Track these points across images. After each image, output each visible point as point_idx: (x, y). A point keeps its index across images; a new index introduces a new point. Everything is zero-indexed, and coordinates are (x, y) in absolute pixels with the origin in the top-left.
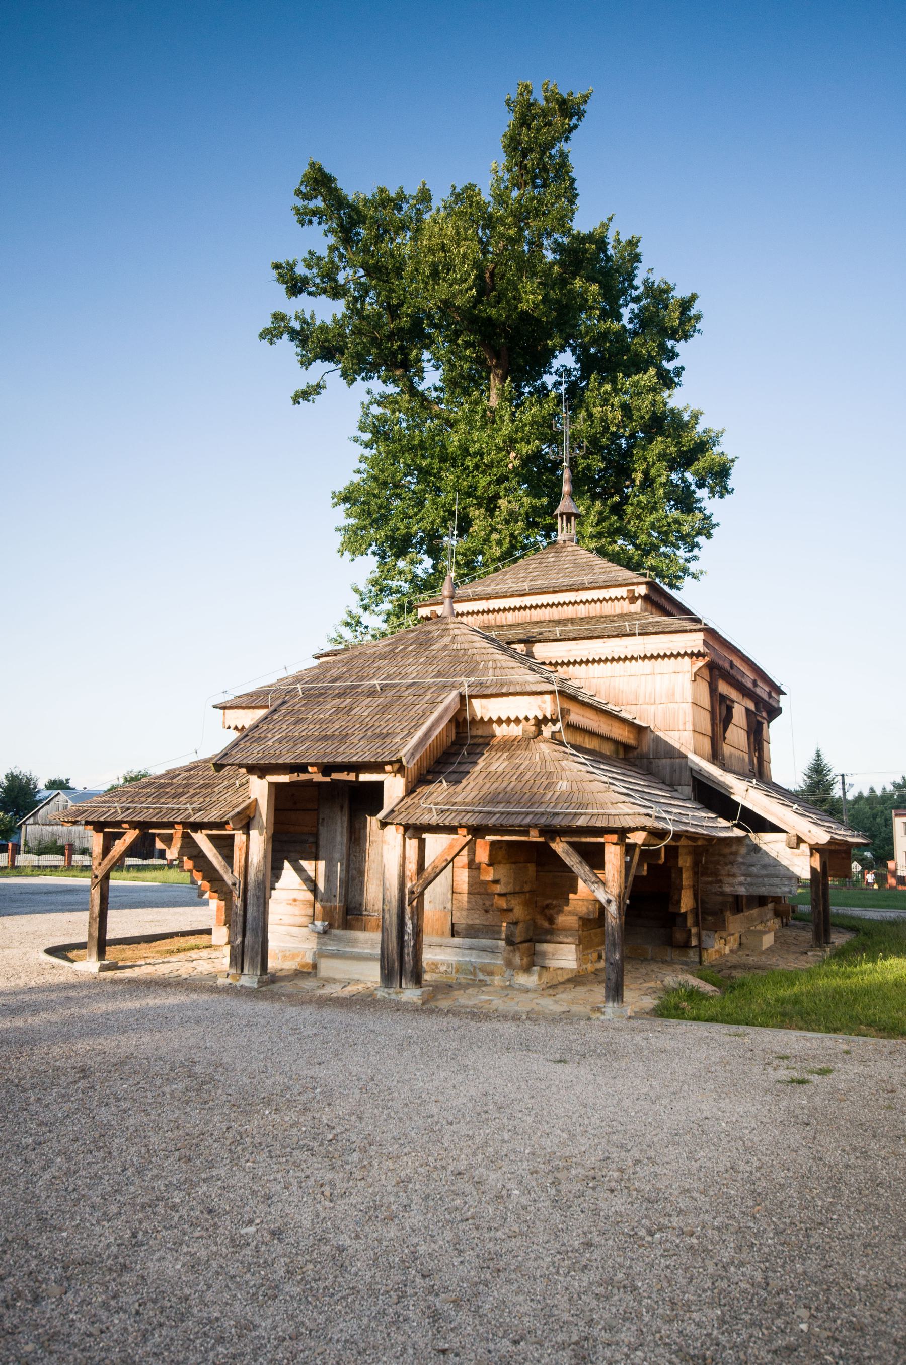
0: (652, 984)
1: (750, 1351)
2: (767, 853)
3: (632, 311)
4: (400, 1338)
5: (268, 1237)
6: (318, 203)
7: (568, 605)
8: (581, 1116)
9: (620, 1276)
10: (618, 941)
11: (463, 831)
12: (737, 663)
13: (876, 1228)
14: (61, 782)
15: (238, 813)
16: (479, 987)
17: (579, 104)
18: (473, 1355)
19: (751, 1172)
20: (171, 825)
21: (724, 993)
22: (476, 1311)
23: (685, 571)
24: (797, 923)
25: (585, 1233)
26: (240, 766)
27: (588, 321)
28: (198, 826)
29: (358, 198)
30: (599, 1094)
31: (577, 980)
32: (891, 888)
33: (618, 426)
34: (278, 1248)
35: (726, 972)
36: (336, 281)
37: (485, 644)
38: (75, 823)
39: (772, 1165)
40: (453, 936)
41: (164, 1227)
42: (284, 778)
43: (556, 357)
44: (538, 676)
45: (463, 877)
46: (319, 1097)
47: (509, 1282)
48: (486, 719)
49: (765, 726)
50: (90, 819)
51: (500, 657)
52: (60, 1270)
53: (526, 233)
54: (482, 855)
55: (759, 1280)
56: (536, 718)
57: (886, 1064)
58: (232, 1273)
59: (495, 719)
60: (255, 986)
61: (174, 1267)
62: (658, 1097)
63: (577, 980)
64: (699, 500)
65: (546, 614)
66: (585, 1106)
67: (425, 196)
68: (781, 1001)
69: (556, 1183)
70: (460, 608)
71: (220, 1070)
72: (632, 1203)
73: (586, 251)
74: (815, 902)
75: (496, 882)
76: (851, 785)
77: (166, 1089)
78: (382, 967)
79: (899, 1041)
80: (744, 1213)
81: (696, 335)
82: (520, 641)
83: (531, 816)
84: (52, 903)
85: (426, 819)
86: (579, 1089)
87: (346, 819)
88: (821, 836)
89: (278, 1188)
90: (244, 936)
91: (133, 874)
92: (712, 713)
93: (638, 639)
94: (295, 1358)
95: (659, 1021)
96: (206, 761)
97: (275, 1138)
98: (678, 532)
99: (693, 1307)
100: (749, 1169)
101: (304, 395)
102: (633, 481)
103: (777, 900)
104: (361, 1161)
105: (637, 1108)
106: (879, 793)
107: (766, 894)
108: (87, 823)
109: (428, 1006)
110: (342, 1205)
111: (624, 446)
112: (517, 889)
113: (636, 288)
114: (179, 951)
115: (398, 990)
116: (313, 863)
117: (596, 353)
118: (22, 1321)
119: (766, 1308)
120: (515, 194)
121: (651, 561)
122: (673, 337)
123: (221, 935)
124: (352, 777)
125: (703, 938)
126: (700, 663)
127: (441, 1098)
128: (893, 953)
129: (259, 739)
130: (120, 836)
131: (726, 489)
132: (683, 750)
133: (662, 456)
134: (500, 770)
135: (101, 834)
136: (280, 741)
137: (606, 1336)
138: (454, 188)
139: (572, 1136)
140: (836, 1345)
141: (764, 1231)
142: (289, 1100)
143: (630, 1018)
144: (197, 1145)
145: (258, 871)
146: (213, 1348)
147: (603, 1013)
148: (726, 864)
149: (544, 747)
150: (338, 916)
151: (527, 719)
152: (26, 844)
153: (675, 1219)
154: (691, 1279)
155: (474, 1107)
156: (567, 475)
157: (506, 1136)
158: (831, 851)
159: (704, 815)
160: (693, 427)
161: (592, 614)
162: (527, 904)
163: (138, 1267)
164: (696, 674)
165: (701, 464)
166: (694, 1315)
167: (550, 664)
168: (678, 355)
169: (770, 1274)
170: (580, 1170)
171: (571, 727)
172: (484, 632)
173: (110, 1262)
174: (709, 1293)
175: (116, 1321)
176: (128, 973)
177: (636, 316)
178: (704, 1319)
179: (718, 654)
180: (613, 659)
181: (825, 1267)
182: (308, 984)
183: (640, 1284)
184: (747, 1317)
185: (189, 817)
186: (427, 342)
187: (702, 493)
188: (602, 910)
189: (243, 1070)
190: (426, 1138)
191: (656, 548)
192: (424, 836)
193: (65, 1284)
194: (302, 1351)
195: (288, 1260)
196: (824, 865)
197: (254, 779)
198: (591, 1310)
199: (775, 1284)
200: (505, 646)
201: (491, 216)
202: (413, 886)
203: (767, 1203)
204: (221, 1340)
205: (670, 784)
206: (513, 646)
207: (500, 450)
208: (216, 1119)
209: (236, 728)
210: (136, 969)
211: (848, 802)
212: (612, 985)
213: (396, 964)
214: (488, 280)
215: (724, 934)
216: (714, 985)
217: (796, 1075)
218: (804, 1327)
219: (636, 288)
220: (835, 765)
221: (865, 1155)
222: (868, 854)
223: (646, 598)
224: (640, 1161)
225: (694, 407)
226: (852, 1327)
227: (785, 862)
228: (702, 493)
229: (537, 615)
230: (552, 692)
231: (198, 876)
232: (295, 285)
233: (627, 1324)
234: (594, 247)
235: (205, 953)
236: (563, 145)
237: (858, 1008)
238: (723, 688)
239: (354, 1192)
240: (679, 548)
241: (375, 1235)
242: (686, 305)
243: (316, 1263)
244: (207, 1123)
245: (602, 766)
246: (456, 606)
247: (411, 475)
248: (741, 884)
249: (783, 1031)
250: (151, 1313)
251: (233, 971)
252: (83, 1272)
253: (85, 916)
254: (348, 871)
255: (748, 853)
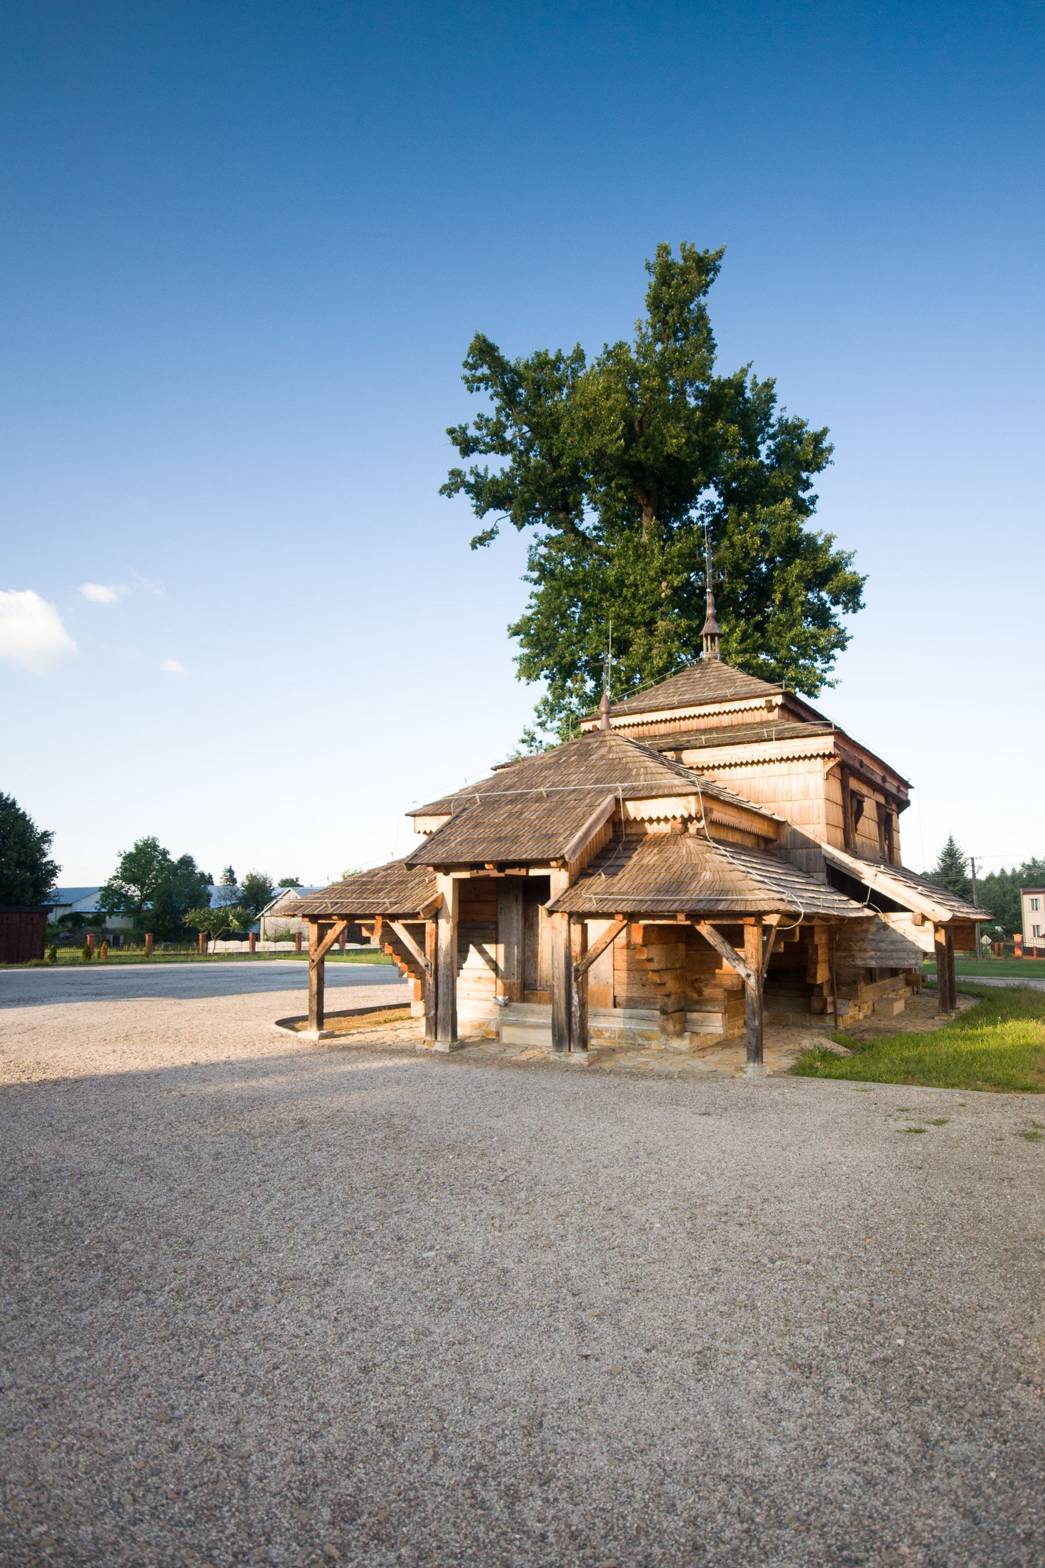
0: (791, 1047)
1: (851, 1361)
2: (894, 931)
3: (769, 448)
4: (550, 1345)
5: (445, 1260)
6: (485, 370)
7: (713, 715)
8: (719, 1161)
9: (742, 1297)
10: (757, 1010)
11: (620, 917)
12: (867, 762)
13: (974, 1258)
14: (292, 881)
15: (428, 906)
16: (638, 1050)
17: (714, 260)
18: (610, 1360)
19: (866, 1210)
20: (372, 916)
21: (854, 1054)
22: (616, 1325)
23: (822, 680)
24: (928, 991)
25: (714, 1260)
26: (428, 865)
27: (729, 459)
28: (394, 917)
29: (518, 363)
30: (737, 1142)
31: (724, 1043)
32: (1018, 958)
33: (758, 551)
34: (453, 1269)
35: (858, 1036)
36: (503, 438)
37: (637, 753)
38: (294, 916)
39: (885, 1204)
40: (615, 1007)
41: (361, 1251)
42: (465, 875)
43: (701, 493)
44: (684, 780)
45: (622, 956)
46: (495, 1144)
47: (646, 1300)
48: (638, 819)
49: (894, 817)
50: (306, 913)
51: (651, 764)
52: (276, 1284)
53: (671, 383)
54: (638, 938)
55: (864, 1301)
56: (682, 816)
57: (998, 1116)
58: (414, 1289)
59: (646, 818)
60: (447, 1050)
61: (368, 1283)
62: (789, 1145)
63: (724, 1043)
64: (834, 616)
65: (693, 724)
66: (724, 1152)
67: (579, 356)
68: (906, 1061)
69: (692, 1218)
70: (616, 722)
71: (414, 1121)
72: (758, 1236)
73: (726, 395)
74: (941, 973)
75: (650, 960)
76: (980, 867)
77: (369, 1138)
78: (554, 1035)
79: (1011, 1095)
80: (856, 1245)
81: (828, 466)
82: (670, 749)
83: (678, 903)
84: (285, 982)
85: (587, 907)
86: (719, 1138)
87: (520, 908)
88: (945, 915)
89: (457, 1219)
90: (437, 1009)
91: (352, 957)
92: (844, 807)
93: (775, 744)
94: (462, 1359)
95: (795, 1079)
96: (400, 861)
97: (456, 1178)
98: (815, 645)
99: (804, 1324)
100: (864, 1207)
101: (481, 541)
102: (773, 601)
103: (908, 971)
104: (527, 1198)
105: (769, 1154)
106: (1009, 872)
107: (894, 966)
108: (304, 916)
109: (593, 1067)
110: (509, 1234)
111: (764, 570)
112: (669, 966)
113: (773, 426)
114: (385, 1022)
115: (568, 1053)
116: (494, 946)
117: (737, 488)
118: (244, 1324)
119: (868, 1326)
120: (659, 347)
121: (791, 673)
122: (806, 470)
123: (418, 1009)
124: (523, 872)
125: (839, 1006)
126: (832, 763)
127: (599, 1145)
128: (1013, 1017)
129: (444, 842)
130: (332, 926)
131: (858, 604)
132: (817, 841)
133: (799, 578)
134: (651, 863)
135: (315, 926)
136: (461, 843)
137: (726, 1347)
138: (606, 346)
139: (710, 1178)
140: (929, 1357)
141: (873, 1260)
142: (470, 1147)
143: (769, 1076)
144: (391, 1184)
145: (446, 954)
146: (395, 1350)
147: (745, 1072)
148: (858, 941)
149: (689, 841)
150: (516, 991)
151: (674, 818)
152: (265, 933)
153: (794, 1249)
154: (805, 1301)
155: (627, 1153)
156: (709, 599)
157: (653, 1178)
158: (956, 928)
159: (837, 898)
160: (827, 550)
161: (735, 722)
162: (677, 978)
163: (338, 1283)
164: (828, 773)
165: (833, 584)
166: (804, 1331)
167: (698, 768)
168: (812, 485)
169: (875, 1297)
170: (714, 1207)
171: (713, 823)
172: (638, 742)
173: (316, 1278)
174: (819, 1312)
175: (319, 1326)
176: (342, 1041)
177: (772, 452)
178: (813, 1334)
179: (848, 755)
180: (753, 763)
181: (925, 1291)
182: (492, 1049)
183: (759, 1304)
184: (851, 1333)
185: (387, 909)
186: (586, 487)
187: (836, 610)
188: (743, 983)
189: (433, 1122)
190: (584, 1179)
191: (795, 661)
192: (586, 921)
193: (280, 1295)
194: (468, 1354)
195: (460, 1279)
196: (949, 939)
197: (440, 876)
198: (715, 1325)
199: (879, 1305)
200: (656, 754)
201: (637, 371)
202: (578, 965)
203: (878, 1236)
204: (402, 1343)
205: (806, 871)
206: (665, 754)
207: (652, 580)
208: (408, 1162)
209: (425, 833)
210: (350, 1037)
211: (980, 882)
212: (753, 1047)
213: (566, 1032)
214: (637, 428)
215: (858, 1002)
216: (846, 1047)
217: (914, 1125)
218: (901, 1342)
219: (773, 426)
220: (966, 850)
221: (971, 1195)
222: (999, 928)
223: (782, 707)
224: (768, 1200)
225: (828, 531)
226: (944, 1342)
227: (911, 938)
228: (836, 610)
229: (685, 725)
230: (696, 794)
231: (397, 959)
232: (468, 446)
233: (745, 1337)
234: (732, 391)
235: (407, 1023)
236: (702, 300)
237: (976, 1066)
238: (854, 784)
239: (520, 1224)
240: (816, 660)
241: (535, 1260)
242: (818, 438)
243: (483, 1282)
244: (400, 1166)
245: (743, 858)
246: (612, 721)
247: (576, 606)
248: (872, 958)
249: (906, 1087)
250: (347, 1320)
251: (428, 1038)
252: (294, 1286)
253: (306, 993)
254: (524, 952)
255: (878, 930)
